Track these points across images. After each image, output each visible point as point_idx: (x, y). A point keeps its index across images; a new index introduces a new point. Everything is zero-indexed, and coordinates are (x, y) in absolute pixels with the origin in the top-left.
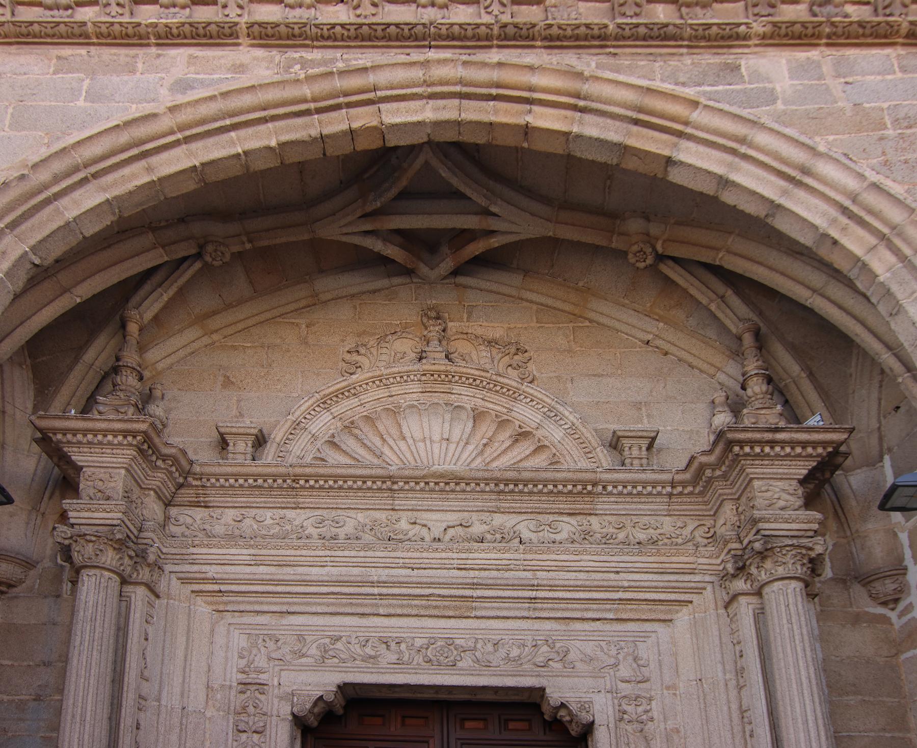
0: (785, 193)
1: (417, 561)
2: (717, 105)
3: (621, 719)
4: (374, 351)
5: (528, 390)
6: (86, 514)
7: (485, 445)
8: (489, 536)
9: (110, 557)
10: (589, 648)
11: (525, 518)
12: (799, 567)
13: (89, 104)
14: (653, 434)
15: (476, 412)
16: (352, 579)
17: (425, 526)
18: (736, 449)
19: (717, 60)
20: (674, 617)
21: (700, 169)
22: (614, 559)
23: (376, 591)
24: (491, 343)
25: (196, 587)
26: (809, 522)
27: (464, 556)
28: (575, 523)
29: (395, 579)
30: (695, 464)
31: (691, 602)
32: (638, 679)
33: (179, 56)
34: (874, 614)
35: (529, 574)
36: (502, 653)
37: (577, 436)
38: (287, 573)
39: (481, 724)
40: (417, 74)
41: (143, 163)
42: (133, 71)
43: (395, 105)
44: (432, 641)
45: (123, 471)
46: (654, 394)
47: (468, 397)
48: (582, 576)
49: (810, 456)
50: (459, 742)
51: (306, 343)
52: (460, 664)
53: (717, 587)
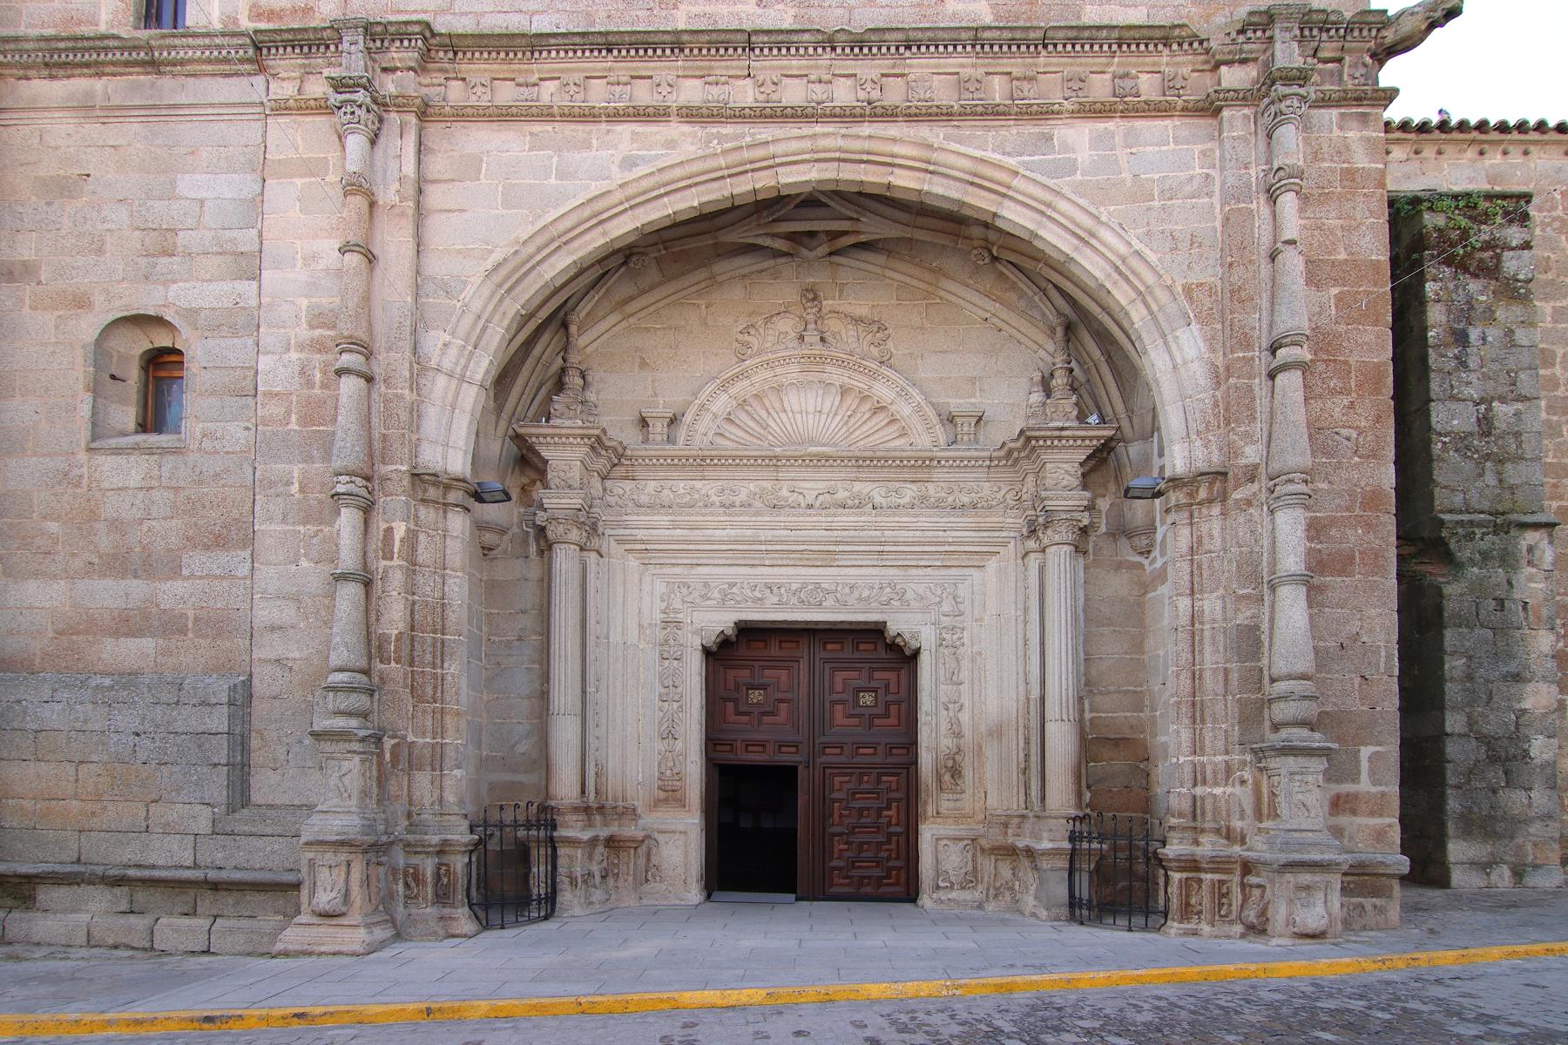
0: (1076, 249)
2: (1032, 175)
9: (575, 534)
10: (921, 589)
19: (1037, 130)
24: (858, 321)
33: (624, 130)
36: (856, 594)
39: (838, 647)
40: (807, 144)
41: (600, 229)
42: (589, 147)
43: (789, 168)
44: (804, 586)
47: (837, 376)
48: (918, 534)
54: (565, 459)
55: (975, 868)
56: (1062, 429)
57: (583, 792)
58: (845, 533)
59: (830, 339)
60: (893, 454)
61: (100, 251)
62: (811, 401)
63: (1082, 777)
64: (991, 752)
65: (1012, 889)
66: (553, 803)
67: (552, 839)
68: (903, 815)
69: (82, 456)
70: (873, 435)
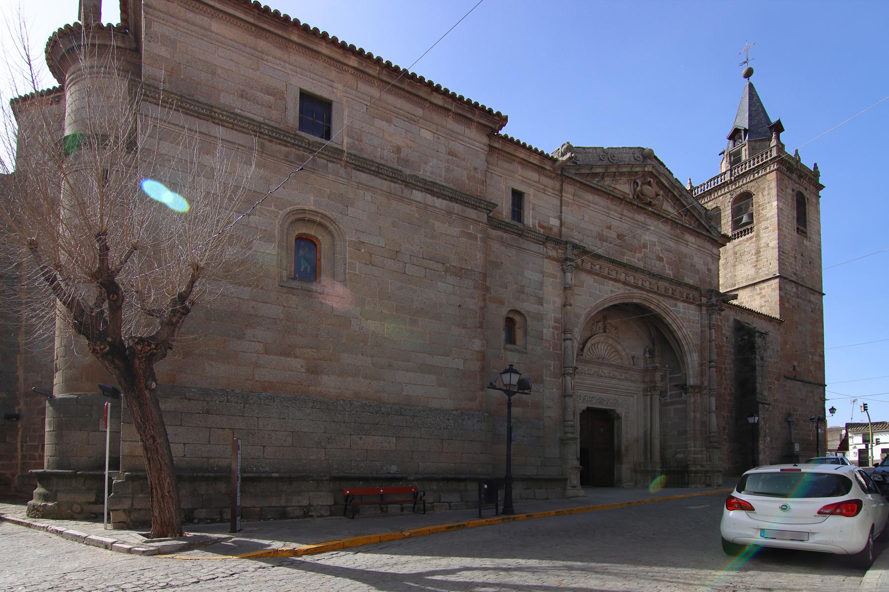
61: (506, 288)
69: (503, 350)
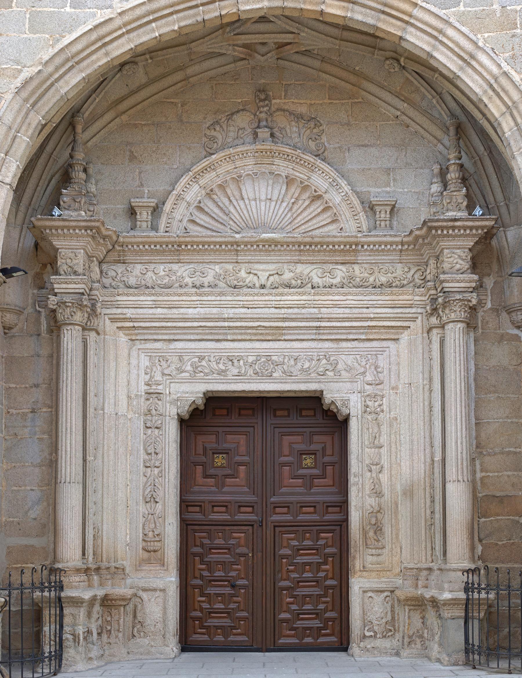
1: (251, 303)
3: (365, 412)
4: (225, 127)
5: (320, 165)
6: (64, 286)
7: (293, 203)
8: (293, 282)
10: (350, 360)
11: (315, 267)
12: (463, 314)
13: (73, 10)
14: (393, 203)
15: (289, 179)
16: (213, 316)
17: (256, 274)
18: (434, 232)
20: (400, 336)
21: (418, 46)
22: (366, 298)
23: (226, 324)
25: (120, 324)
26: (470, 282)
27: (278, 298)
28: (344, 270)
29: (238, 316)
30: (413, 235)
31: (409, 327)
32: (377, 382)
34: (512, 335)
35: (316, 310)
37: (349, 202)
38: (175, 313)
39: (286, 413)
41: (103, 51)
45: (82, 251)
46: (399, 161)
47: (283, 168)
48: (347, 311)
49: (475, 235)
50: (273, 426)
51: (182, 121)
52: (274, 375)
53: (424, 317)
54: (73, 252)
55: (393, 618)
56: (455, 220)
57: (84, 554)
58: (290, 311)
59: (278, 134)
60: (327, 240)
62: (263, 190)
63: (475, 533)
64: (404, 510)
65: (421, 637)
66: (60, 566)
67: (60, 599)
68: (337, 571)
70: (312, 223)
